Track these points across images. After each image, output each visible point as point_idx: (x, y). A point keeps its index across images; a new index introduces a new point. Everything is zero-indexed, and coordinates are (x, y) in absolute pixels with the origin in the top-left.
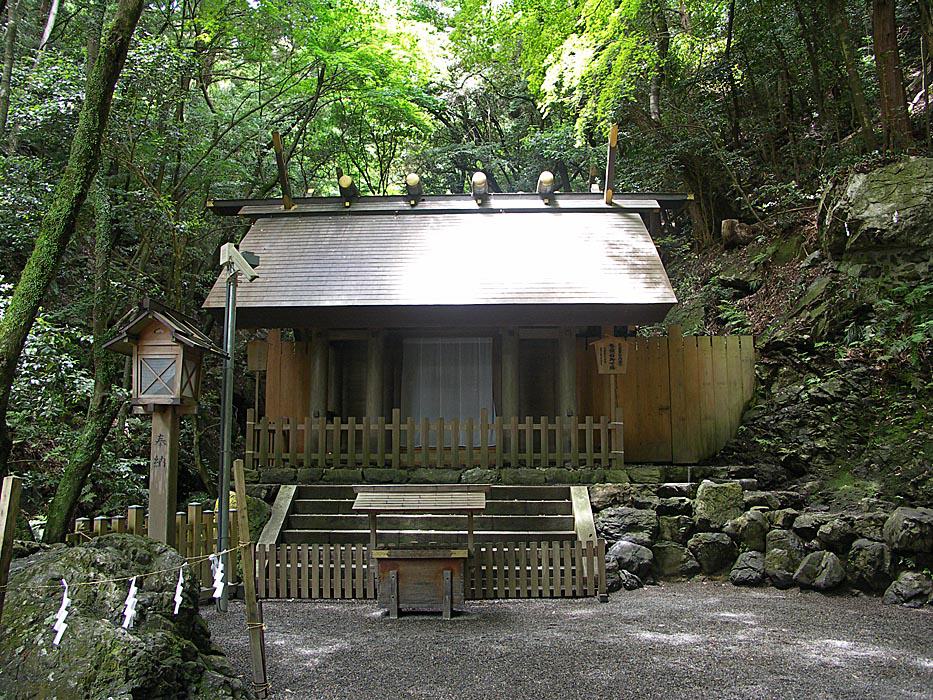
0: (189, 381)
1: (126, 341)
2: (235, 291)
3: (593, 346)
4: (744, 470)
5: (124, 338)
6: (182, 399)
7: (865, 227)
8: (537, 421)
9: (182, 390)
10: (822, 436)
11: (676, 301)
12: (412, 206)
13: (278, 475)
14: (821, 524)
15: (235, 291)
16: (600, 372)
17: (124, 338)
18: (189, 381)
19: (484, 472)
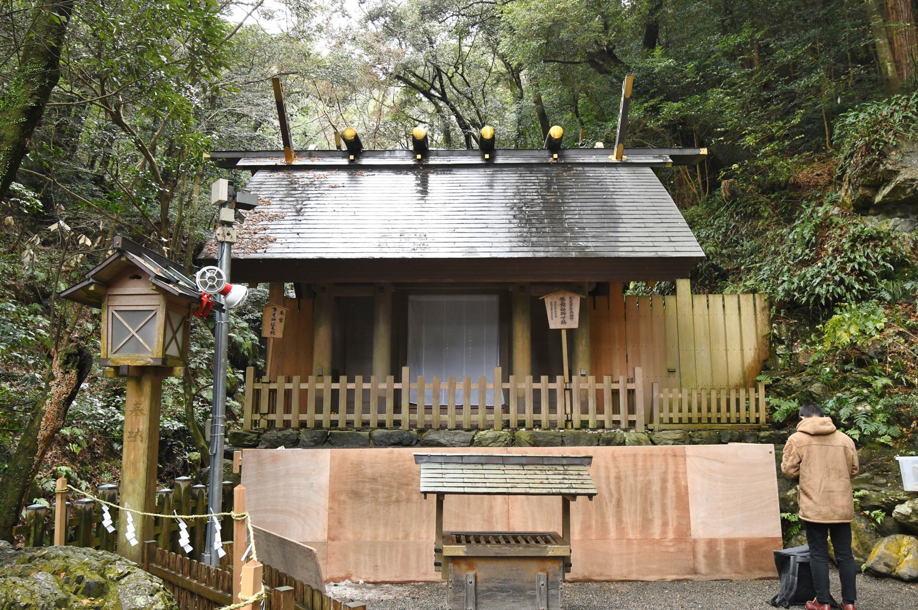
0: (174, 337)
1: (92, 288)
2: (311, 154)
3: (543, 300)
4: (775, 434)
5: (91, 284)
6: (165, 358)
7: (900, 178)
8: (552, 380)
9: (165, 348)
10: (865, 400)
11: (703, 254)
12: (351, 161)
13: (279, 437)
14: (897, 504)
15: (311, 154)
16: (552, 326)
17: (91, 284)
18: (174, 337)
19: (498, 433)
